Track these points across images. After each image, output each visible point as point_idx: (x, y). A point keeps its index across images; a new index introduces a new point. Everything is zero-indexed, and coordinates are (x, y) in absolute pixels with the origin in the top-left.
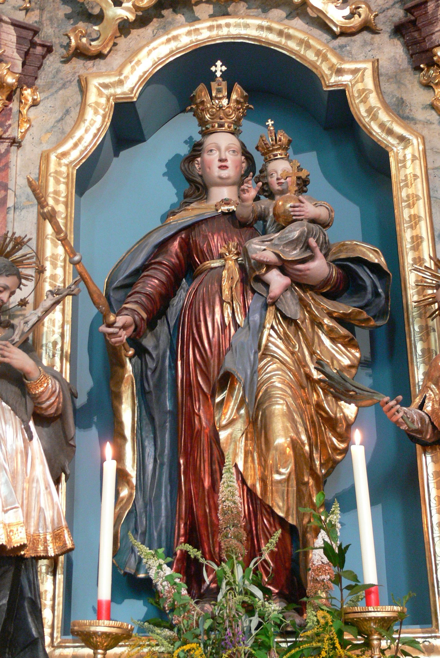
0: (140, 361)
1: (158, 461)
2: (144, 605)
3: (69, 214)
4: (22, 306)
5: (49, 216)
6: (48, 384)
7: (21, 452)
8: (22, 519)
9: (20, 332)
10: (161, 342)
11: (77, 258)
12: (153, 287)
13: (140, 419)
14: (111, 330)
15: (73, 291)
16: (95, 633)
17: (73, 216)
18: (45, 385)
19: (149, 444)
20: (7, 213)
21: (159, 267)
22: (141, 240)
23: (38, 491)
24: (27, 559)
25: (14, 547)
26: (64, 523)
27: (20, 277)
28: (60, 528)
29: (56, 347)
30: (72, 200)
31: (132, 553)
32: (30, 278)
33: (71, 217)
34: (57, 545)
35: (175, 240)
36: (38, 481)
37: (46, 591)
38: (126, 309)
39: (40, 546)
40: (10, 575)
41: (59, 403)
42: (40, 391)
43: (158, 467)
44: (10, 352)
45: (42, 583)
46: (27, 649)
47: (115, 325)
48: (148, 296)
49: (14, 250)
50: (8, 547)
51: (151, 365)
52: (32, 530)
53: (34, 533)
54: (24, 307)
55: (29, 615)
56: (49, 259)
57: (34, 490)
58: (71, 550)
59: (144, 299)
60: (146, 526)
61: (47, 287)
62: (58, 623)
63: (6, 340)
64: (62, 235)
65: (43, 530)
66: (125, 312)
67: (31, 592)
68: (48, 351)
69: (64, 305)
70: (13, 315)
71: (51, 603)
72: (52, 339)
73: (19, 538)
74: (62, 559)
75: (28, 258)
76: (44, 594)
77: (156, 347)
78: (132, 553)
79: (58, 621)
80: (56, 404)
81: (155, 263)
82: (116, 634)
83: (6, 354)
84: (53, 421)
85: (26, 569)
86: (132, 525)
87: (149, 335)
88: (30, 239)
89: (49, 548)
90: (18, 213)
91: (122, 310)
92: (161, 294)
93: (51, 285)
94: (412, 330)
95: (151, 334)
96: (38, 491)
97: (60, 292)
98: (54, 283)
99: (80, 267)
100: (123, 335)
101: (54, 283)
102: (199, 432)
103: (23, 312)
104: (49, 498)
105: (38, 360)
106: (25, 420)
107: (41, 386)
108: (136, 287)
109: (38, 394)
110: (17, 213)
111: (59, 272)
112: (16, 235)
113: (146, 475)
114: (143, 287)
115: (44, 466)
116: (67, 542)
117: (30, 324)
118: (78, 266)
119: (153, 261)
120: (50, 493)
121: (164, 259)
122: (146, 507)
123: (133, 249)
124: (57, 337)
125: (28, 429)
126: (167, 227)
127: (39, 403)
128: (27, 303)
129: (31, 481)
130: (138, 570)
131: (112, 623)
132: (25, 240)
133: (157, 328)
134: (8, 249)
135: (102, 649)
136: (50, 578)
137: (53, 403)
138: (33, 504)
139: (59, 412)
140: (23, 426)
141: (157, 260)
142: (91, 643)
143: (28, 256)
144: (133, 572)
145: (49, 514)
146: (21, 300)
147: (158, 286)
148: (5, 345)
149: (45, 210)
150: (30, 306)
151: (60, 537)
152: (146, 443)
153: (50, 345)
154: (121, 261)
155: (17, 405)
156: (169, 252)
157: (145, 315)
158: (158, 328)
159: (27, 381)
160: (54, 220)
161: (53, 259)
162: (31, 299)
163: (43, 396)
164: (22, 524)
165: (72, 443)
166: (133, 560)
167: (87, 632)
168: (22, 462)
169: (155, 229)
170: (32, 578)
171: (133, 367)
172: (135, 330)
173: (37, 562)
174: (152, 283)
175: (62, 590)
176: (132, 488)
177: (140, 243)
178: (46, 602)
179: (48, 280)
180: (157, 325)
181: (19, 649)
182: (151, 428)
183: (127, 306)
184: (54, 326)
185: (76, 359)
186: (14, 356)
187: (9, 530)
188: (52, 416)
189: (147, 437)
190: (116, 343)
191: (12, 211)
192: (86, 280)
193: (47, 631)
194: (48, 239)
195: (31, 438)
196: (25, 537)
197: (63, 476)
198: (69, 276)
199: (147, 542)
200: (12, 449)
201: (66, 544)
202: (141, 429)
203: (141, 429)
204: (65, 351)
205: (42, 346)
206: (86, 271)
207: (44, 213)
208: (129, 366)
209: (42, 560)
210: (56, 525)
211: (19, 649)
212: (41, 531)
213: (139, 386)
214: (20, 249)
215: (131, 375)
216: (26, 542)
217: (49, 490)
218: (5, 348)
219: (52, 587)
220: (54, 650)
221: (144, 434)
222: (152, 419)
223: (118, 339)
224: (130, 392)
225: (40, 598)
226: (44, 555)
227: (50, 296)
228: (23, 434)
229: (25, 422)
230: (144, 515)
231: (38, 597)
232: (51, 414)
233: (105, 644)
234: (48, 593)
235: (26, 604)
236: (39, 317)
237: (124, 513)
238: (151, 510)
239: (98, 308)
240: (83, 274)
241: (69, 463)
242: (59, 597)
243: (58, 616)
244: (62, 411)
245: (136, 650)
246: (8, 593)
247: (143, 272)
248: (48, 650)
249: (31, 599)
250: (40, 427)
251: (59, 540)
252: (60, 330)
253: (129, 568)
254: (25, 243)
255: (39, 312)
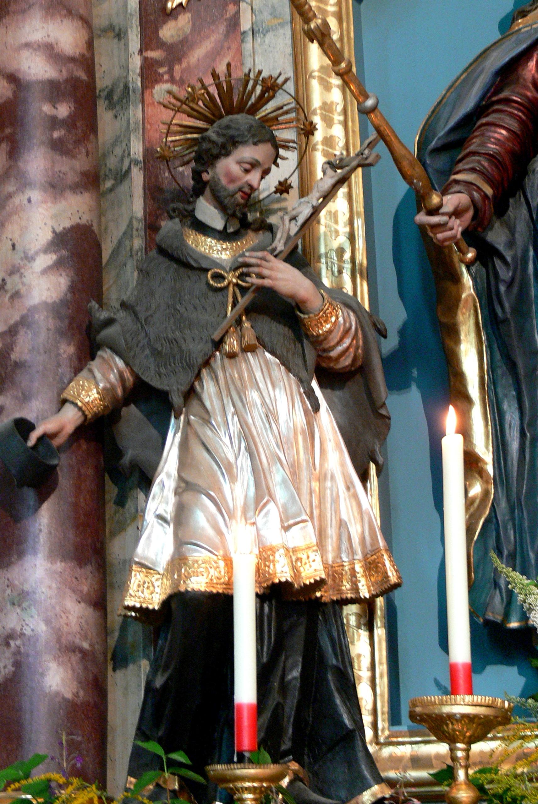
0: (484, 271)
1: (528, 435)
2: (520, 674)
3: (345, 33)
4: (281, 194)
5: (319, 35)
6: (337, 318)
7: (303, 431)
8: (314, 540)
9: (285, 235)
10: (517, 236)
11: (370, 103)
12: (498, 142)
13: (492, 367)
14: (435, 219)
15: (366, 158)
16: (451, 717)
17: (352, 35)
18: (333, 319)
19: (510, 406)
20: (242, 41)
21: (506, 108)
22: (471, 65)
23: (334, 494)
24: (325, 604)
25: (304, 584)
26: (381, 543)
27: (276, 145)
28: (376, 551)
29: (342, 256)
30: (347, 8)
31: (495, 588)
32: (291, 144)
33: (349, 38)
34: (373, 579)
35: (530, 58)
36: (333, 478)
37: (359, 656)
38: (457, 182)
39: (345, 583)
40: (301, 631)
41: (357, 348)
42: (325, 329)
43: (528, 443)
44: (271, 269)
45: (353, 643)
46: (337, 748)
47: (442, 211)
48: (491, 157)
49: (263, 100)
50: (296, 586)
51: (505, 274)
52: (330, 557)
53: (333, 562)
54: (285, 195)
55: (336, 695)
56: (318, 111)
57: (328, 492)
58: (397, 586)
59: (486, 164)
60: (515, 545)
61: (319, 160)
62: (383, 707)
63: (263, 249)
64: (343, 65)
65: (348, 557)
66: (456, 188)
67: (337, 659)
68: (329, 264)
69: (350, 187)
70: (267, 211)
71: (369, 674)
72: (335, 245)
73: (312, 570)
74: (380, 602)
75: (287, 112)
76: (356, 660)
77: (511, 244)
78: (495, 588)
79: (383, 702)
80: (351, 350)
81: (499, 102)
82: (486, 717)
83: (266, 272)
84: (348, 379)
85: (326, 620)
86: (492, 542)
87: (497, 225)
88: (286, 80)
89: (360, 585)
90: (259, 40)
91: (450, 184)
92: (512, 153)
93: (326, 153)
94: (490, 428)
95: (501, 224)
96: (334, 494)
97: (344, 163)
98: (330, 150)
99: (376, 116)
100: (455, 227)
101: (330, 150)
102: (105, 99)
103: (283, 205)
104: (354, 504)
105: (316, 280)
106: (303, 379)
107: (326, 322)
108: (470, 145)
109: (323, 334)
110: (259, 40)
111: (338, 131)
112: (264, 74)
113: (509, 458)
114: (483, 144)
115: (341, 451)
116: (390, 574)
117: (301, 219)
118: (373, 116)
119: (494, 99)
120: (355, 496)
121: (513, 91)
122: (512, 511)
123: (459, 81)
124: (342, 240)
125: (310, 394)
126: (514, 38)
127: (325, 350)
128: (290, 186)
129: (322, 478)
130: (507, 616)
131: (477, 699)
132: (280, 80)
133: (509, 212)
134: (253, 99)
135: (463, 743)
136: (364, 634)
137: (348, 349)
138: (329, 515)
139: (359, 363)
140: (302, 390)
141: (502, 95)
142: (443, 732)
143: (285, 108)
144: (499, 618)
145: (355, 530)
146: (280, 183)
147: (507, 139)
148: (263, 259)
149: (312, 25)
150: (294, 192)
151: (377, 567)
152: (505, 406)
153: (334, 255)
154: (439, 103)
155: (290, 356)
156: (521, 80)
157: (489, 191)
158: (511, 212)
159: (302, 315)
160: (327, 41)
161: (325, 110)
162: (294, 181)
163: (331, 337)
164: (315, 548)
165: (383, 412)
166: (497, 599)
167: (436, 715)
168: (305, 448)
169: (494, 44)
170: (335, 634)
171: (474, 279)
172: (474, 218)
173: (341, 609)
174: (496, 135)
175: (384, 653)
176: (487, 482)
177: (470, 70)
178: (360, 673)
179: (320, 147)
180: (508, 207)
181: (324, 749)
182: (511, 381)
183: (459, 177)
184: (336, 222)
185: (375, 274)
186: (280, 275)
187: (294, 558)
188: (347, 370)
189: (506, 396)
190: (445, 240)
191: (250, 38)
192: (388, 139)
193: (367, 719)
194: (314, 77)
195: (316, 408)
196: (322, 568)
197: (373, 467)
198: (353, 137)
199: (518, 567)
200: (288, 427)
201: (388, 577)
202: (495, 385)
203: (495, 385)
204: (357, 262)
205: (319, 257)
206: (387, 124)
207: (310, 30)
208: (467, 280)
209: (350, 606)
210: (369, 547)
211: (324, 749)
212: (345, 559)
213: (486, 312)
214: (273, 97)
215: (472, 295)
216: (323, 576)
217: (352, 490)
218: (264, 263)
219: (369, 648)
220: (380, 749)
221: (499, 390)
222: (512, 366)
223: (448, 234)
224: (472, 322)
225: (352, 667)
226: (353, 596)
227: (330, 172)
228: (303, 403)
229: (304, 383)
230: (510, 526)
231: (348, 664)
232: (347, 367)
233: (468, 734)
234: (362, 658)
235: (330, 677)
236: (313, 207)
237: (477, 523)
238: (521, 518)
239: (410, 183)
240: (382, 129)
241: (381, 446)
242: (381, 663)
243: (382, 695)
244: (363, 362)
245: (517, 743)
246: (301, 659)
247: (479, 118)
248: (371, 749)
249: (337, 668)
250: (329, 391)
251: (376, 572)
252: (347, 229)
253: (493, 613)
254: (280, 87)
255: (314, 198)
